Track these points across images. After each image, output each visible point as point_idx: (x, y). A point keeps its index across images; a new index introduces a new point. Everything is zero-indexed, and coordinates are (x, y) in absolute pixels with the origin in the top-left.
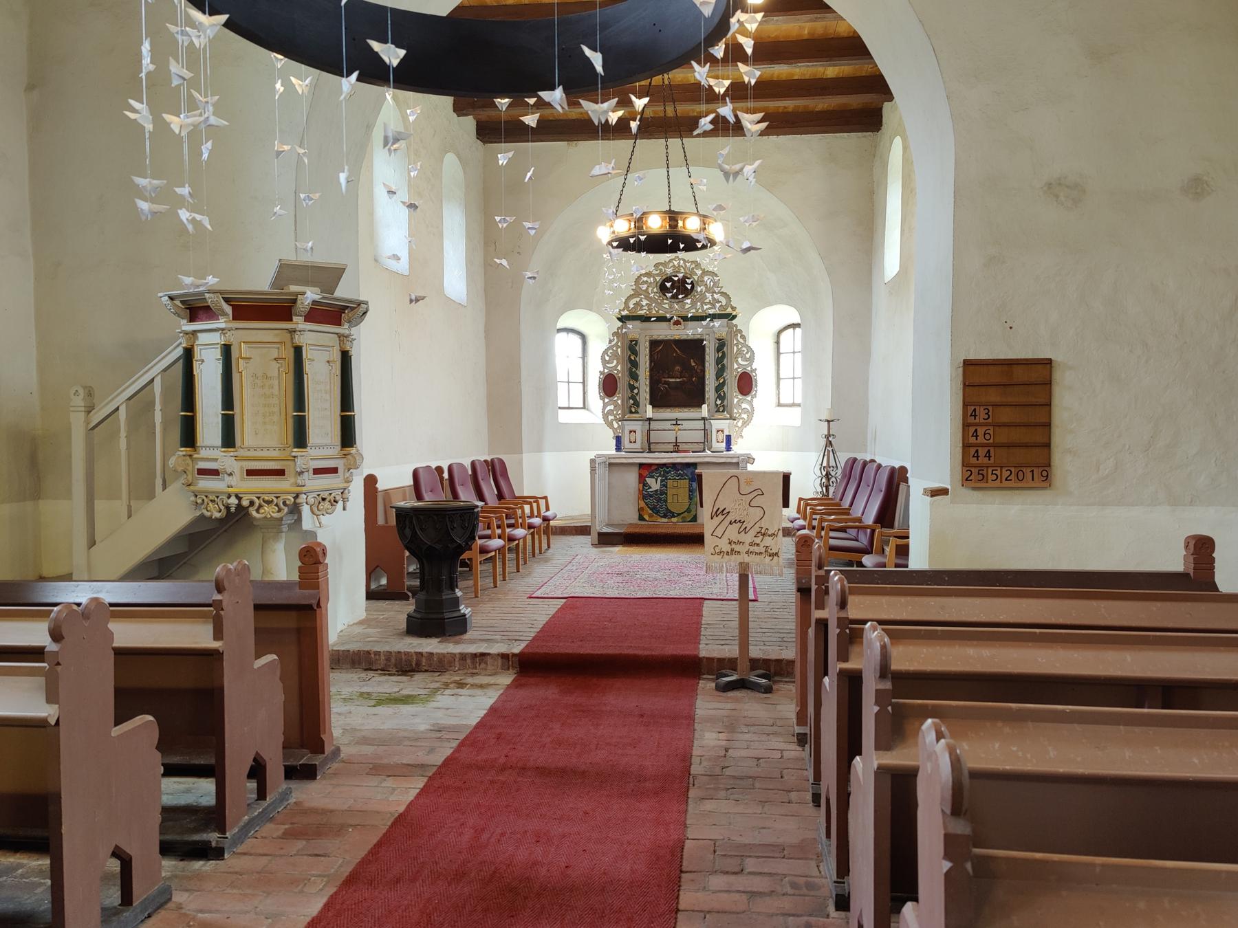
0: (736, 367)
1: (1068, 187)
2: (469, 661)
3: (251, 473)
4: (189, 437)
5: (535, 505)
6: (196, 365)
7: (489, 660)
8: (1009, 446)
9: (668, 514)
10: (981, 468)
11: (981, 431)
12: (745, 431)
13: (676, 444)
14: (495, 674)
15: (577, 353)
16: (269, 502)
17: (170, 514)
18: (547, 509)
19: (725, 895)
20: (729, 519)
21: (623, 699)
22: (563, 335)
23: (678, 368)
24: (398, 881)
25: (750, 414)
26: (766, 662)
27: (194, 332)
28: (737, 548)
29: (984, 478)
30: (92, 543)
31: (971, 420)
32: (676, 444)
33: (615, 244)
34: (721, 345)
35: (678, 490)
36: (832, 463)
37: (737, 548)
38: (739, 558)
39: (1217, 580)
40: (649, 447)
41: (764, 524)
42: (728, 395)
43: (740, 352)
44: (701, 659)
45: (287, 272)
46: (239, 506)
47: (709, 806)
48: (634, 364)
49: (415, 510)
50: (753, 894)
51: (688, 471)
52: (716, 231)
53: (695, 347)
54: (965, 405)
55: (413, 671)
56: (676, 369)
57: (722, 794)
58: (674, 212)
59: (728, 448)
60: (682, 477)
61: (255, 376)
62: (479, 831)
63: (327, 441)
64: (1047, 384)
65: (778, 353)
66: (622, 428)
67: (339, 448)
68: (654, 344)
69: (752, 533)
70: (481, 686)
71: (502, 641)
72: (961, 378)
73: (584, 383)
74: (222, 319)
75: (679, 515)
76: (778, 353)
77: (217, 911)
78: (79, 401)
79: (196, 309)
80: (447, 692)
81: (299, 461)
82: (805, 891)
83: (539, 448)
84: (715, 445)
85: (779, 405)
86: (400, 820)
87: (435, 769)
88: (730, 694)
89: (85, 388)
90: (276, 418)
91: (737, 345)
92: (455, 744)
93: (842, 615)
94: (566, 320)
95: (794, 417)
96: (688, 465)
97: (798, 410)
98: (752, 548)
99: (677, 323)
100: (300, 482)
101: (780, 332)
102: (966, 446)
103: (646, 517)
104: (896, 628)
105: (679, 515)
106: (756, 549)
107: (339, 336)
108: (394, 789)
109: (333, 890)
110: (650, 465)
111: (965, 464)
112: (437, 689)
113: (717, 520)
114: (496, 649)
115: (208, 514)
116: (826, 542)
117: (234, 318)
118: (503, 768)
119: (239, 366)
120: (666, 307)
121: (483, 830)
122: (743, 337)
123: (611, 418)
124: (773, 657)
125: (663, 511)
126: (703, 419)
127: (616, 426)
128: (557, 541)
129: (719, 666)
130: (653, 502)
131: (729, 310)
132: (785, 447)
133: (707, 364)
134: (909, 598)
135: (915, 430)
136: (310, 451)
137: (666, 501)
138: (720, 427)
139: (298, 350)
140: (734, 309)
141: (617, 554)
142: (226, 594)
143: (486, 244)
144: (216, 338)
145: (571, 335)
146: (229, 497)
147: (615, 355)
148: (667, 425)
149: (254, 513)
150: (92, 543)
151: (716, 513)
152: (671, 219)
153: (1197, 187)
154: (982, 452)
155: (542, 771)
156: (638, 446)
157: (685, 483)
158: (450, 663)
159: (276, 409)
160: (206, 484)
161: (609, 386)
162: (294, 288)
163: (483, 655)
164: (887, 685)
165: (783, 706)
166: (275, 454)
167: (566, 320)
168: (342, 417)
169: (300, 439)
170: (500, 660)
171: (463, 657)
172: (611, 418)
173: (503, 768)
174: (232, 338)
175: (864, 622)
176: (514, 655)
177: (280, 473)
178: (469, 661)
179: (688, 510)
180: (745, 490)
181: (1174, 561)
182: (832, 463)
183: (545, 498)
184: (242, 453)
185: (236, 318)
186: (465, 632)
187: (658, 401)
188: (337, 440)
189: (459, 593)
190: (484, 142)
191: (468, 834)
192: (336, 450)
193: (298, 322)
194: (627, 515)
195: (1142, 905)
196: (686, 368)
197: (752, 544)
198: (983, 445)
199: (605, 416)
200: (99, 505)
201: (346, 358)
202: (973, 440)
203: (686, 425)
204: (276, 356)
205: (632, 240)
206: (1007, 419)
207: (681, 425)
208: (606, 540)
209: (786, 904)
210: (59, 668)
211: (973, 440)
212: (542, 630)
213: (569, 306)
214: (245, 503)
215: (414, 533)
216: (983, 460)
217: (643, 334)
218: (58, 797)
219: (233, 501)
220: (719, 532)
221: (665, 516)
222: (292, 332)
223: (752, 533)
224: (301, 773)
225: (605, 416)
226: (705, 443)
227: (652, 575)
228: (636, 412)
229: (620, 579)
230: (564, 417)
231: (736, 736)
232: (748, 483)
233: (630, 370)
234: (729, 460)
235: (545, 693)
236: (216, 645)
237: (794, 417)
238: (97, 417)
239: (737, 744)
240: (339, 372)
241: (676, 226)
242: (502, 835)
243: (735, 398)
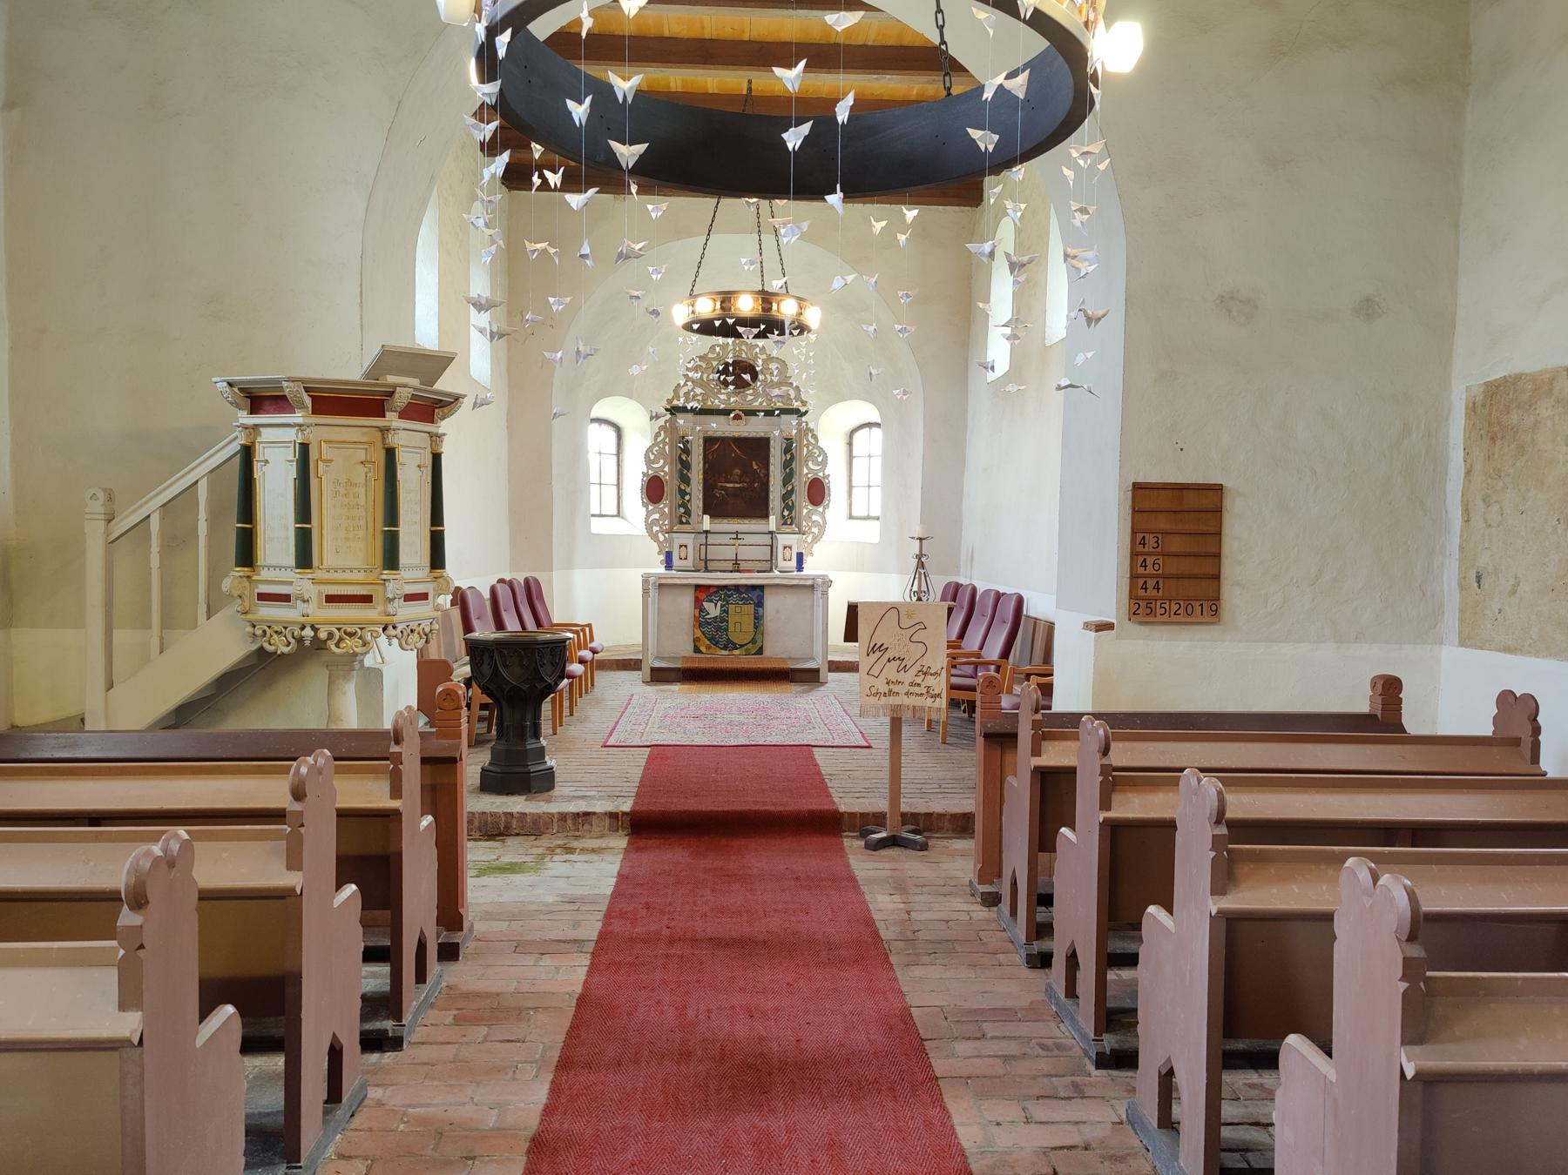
0: (807, 471)
2: (569, 822)
3: (331, 599)
4: (246, 554)
6: (257, 467)
7: (594, 820)
8: (1178, 577)
9: (730, 645)
10: (1149, 601)
11: (1150, 560)
12: (817, 548)
13: (736, 562)
14: (602, 837)
15: (617, 449)
16: (351, 635)
17: (218, 646)
18: (592, 640)
19: (977, 1061)
20: (887, 656)
21: (766, 860)
22: (595, 425)
23: (737, 471)
24: (619, 1064)
26: (915, 816)
27: (256, 426)
28: (895, 688)
29: (1152, 612)
30: (110, 686)
31: (1140, 548)
32: (736, 562)
33: (696, 326)
35: (740, 616)
36: (924, 588)
37: (895, 688)
38: (893, 700)
39: (1404, 721)
40: (706, 565)
41: (926, 662)
43: (810, 455)
44: (842, 814)
45: (391, 359)
46: (315, 637)
47: (917, 972)
48: (686, 465)
49: (497, 642)
50: (1007, 1058)
51: (754, 595)
52: (813, 317)
53: (759, 447)
54: (1134, 532)
55: (501, 834)
56: (734, 473)
57: (926, 959)
58: (767, 293)
59: (800, 568)
60: (746, 601)
61: (337, 482)
62: (682, 1009)
63: (416, 561)
64: (1218, 511)
65: (851, 457)
68: (709, 441)
69: (913, 671)
70: (593, 851)
71: (601, 798)
72: (1129, 502)
74: (299, 414)
76: (851, 457)
77: (427, 1105)
78: (97, 507)
79: (260, 399)
80: (556, 858)
81: (390, 586)
82: (1056, 1052)
83: (569, 565)
85: (851, 517)
86: (582, 1001)
87: (593, 945)
88: (884, 852)
89: (105, 490)
90: (361, 533)
92: (600, 916)
93: (1105, 761)
94: (601, 409)
95: (871, 533)
96: (754, 587)
97: (877, 523)
98: (912, 689)
99: (737, 417)
100: (390, 610)
101: (853, 432)
102: (1134, 577)
103: (703, 649)
104: (1234, 777)
106: (916, 690)
107: (431, 435)
108: (557, 969)
109: (551, 1077)
110: (709, 587)
111: (1133, 596)
112: (543, 856)
114: (601, 807)
115: (270, 649)
116: (948, 680)
117: (314, 412)
118: (672, 941)
119: (319, 470)
120: (724, 397)
121: (685, 1007)
122: (815, 437)
123: (656, 529)
124: (922, 810)
125: (723, 641)
127: (661, 538)
129: (864, 823)
130: (712, 631)
131: (796, 404)
132: (859, 567)
134: (1127, 743)
135: (1051, 551)
136: (403, 574)
139: (390, 453)
140: (804, 403)
141: (678, 695)
142: (404, 744)
144: (290, 435)
145: (605, 427)
146: (303, 628)
147: (661, 454)
148: (726, 539)
149: (333, 648)
150: (110, 686)
152: (764, 300)
153: (1368, 308)
154: (1151, 583)
155: (717, 942)
156: (689, 563)
158: (546, 823)
159: (362, 523)
160: (268, 611)
161: (654, 490)
162: (391, 379)
163: (587, 814)
164: (1223, 830)
165: (957, 860)
166: (360, 576)
167: (601, 409)
168: (433, 533)
169: (391, 559)
170: (607, 821)
171: (563, 817)
172: (656, 529)
173: (672, 941)
174: (312, 436)
175: (1182, 770)
176: (624, 814)
177: (367, 599)
178: (569, 822)
179: (753, 641)
180: (906, 623)
181: (1361, 703)
182: (924, 588)
183: (589, 626)
184: (320, 575)
185: (316, 411)
186: (552, 787)
187: (714, 507)
188: (427, 561)
189: (544, 742)
190: (510, 188)
191: (671, 1014)
192: (424, 572)
193: (392, 419)
194: (680, 647)
195: (1557, 1011)
196: (747, 472)
197: (912, 684)
198: (1151, 576)
200: (120, 636)
201: (436, 459)
202: (1141, 570)
203: (748, 539)
204: (363, 458)
205: (717, 323)
206: (1176, 549)
207: (739, 539)
208: (660, 676)
209: (1044, 1065)
210: (302, 830)
211: (1141, 570)
212: (642, 785)
213: (605, 392)
214: (323, 635)
215: (496, 671)
216: (1151, 592)
217: (696, 430)
218: (298, 977)
219: (308, 632)
220: (875, 671)
221: (725, 648)
222: (385, 431)
223: (913, 671)
224: (449, 953)
225: (649, 526)
227: (735, 718)
229: (698, 723)
230: (597, 526)
231: (912, 898)
232: (909, 616)
233: (681, 472)
235: (672, 857)
236: (395, 804)
238: (120, 527)
239: (917, 907)
240: (429, 479)
243: (805, 508)
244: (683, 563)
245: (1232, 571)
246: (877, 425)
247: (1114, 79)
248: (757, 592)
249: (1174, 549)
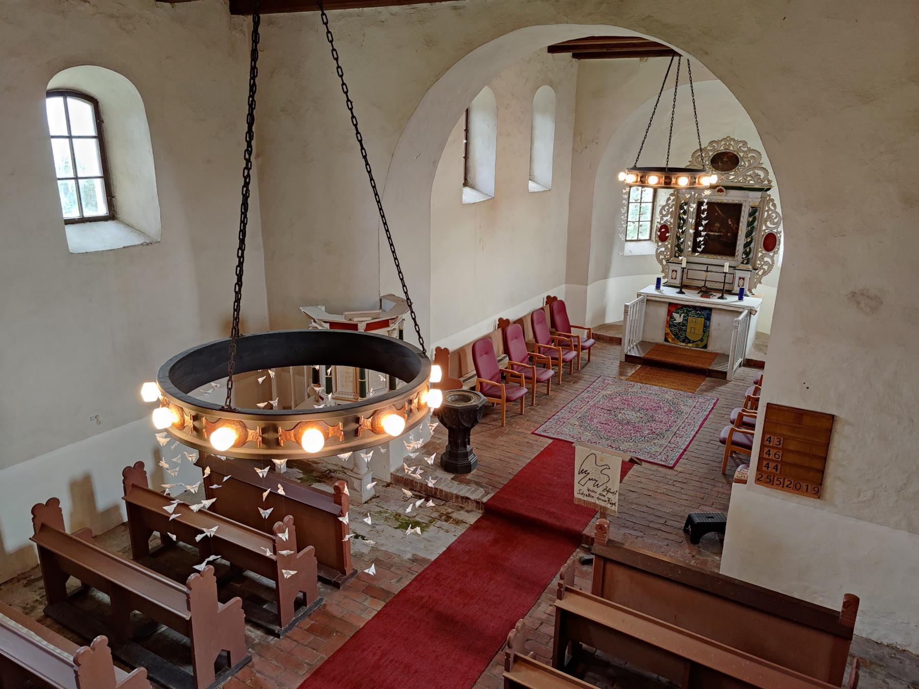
0: (766, 228)
1: (868, 297)
9: (686, 340)
11: (773, 452)
23: (718, 225)
28: (592, 494)
31: (767, 443)
34: (754, 211)
35: (695, 324)
37: (592, 494)
41: (609, 485)
44: (582, 535)
51: (705, 313)
64: (829, 432)
67: (388, 389)
69: (601, 488)
91: (768, 211)
99: (721, 191)
103: (670, 340)
106: (602, 498)
110: (677, 305)
123: (661, 257)
125: (682, 337)
130: (676, 331)
137: (685, 331)
143: (575, 135)
151: (581, 472)
154: (772, 465)
157: (702, 320)
161: (662, 234)
172: (661, 257)
179: (702, 340)
198: (773, 448)
220: (583, 482)
221: (683, 342)
223: (601, 488)
242: (392, 661)
245: (832, 468)
247: (445, 399)
248: (708, 312)
249: (791, 448)
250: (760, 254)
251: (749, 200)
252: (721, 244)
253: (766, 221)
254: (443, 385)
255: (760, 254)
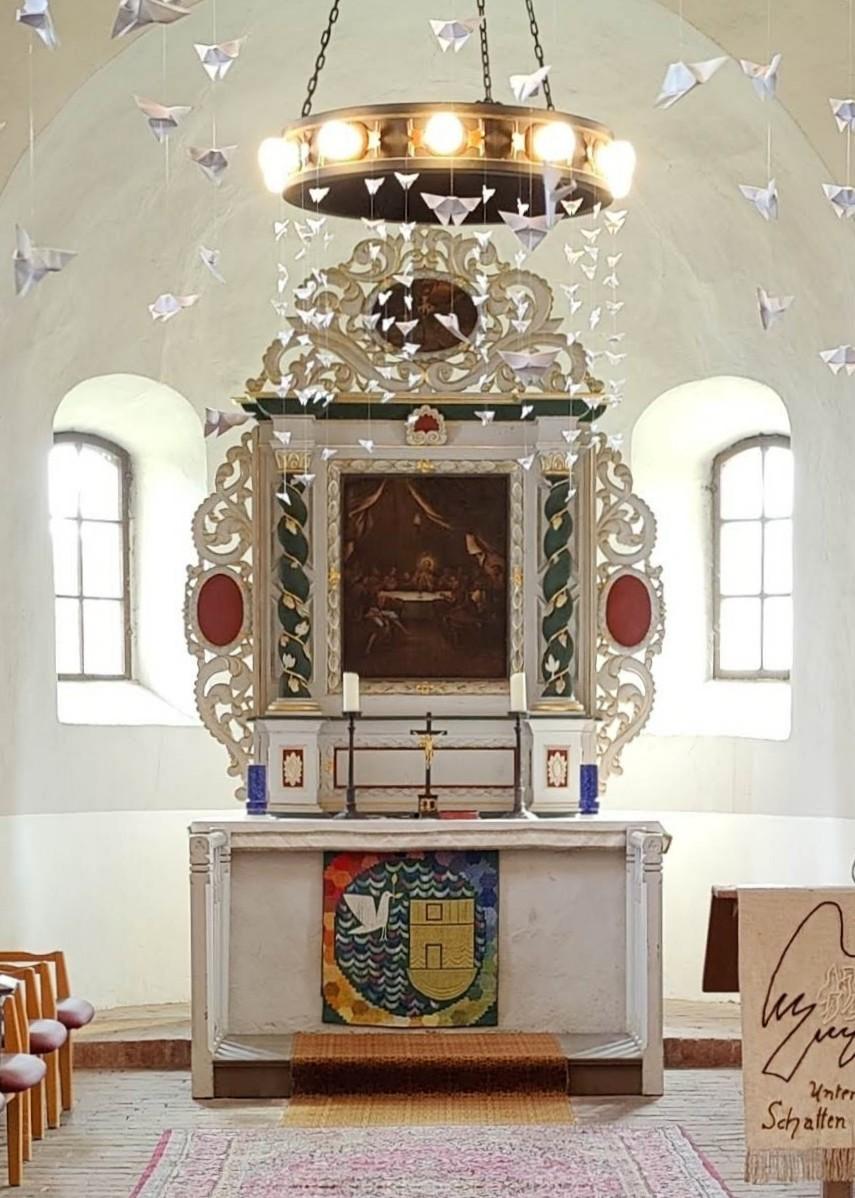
0: (603, 559)
5: (37, 977)
9: (413, 1003)
12: (631, 754)
13: (428, 791)
18: (64, 993)
20: (813, 1025)
22: (67, 449)
23: (427, 561)
25: (645, 702)
32: (428, 791)
33: (318, 195)
35: (440, 928)
40: (350, 801)
42: (580, 645)
48: (297, 547)
51: (473, 874)
52: (615, 167)
53: (481, 498)
58: (498, 108)
59: (589, 804)
60: (453, 890)
66: (260, 741)
68: (355, 485)
73: (126, 599)
75: (444, 1004)
84: (543, 795)
85: (717, 674)
91: (604, 495)
94: (79, 408)
95: (768, 713)
101: (719, 459)
103: (346, 1013)
105: (444, 1004)
113: (778, 1029)
120: (390, 375)
122: (624, 472)
123: (222, 709)
125: (395, 993)
126: (515, 716)
127: (237, 732)
128: (91, 1090)
130: (369, 969)
131: (575, 390)
133: (515, 551)
137: (405, 964)
138: (558, 742)
140: (595, 387)
148: (401, 734)
152: (491, 126)
156: (308, 796)
157: (463, 909)
161: (216, 610)
167: (79, 408)
172: (222, 709)
179: (473, 992)
187: (370, 654)
194: (288, 1010)
196: (453, 561)
199: (205, 703)
203: (457, 733)
205: (373, 186)
207: (433, 737)
208: (236, 1083)
217: (320, 457)
221: (402, 1009)
226: (514, 795)
228: (303, 693)
230: (76, 705)
233: (284, 564)
234: (595, 841)
237: (768, 713)
241: (508, 147)
243: (600, 652)
244: (293, 795)
246: (782, 439)
248: (483, 868)
250: (601, 660)
251: (524, 458)
252: (456, 636)
253: (603, 532)
254: (456, 579)
255: (601, 660)
